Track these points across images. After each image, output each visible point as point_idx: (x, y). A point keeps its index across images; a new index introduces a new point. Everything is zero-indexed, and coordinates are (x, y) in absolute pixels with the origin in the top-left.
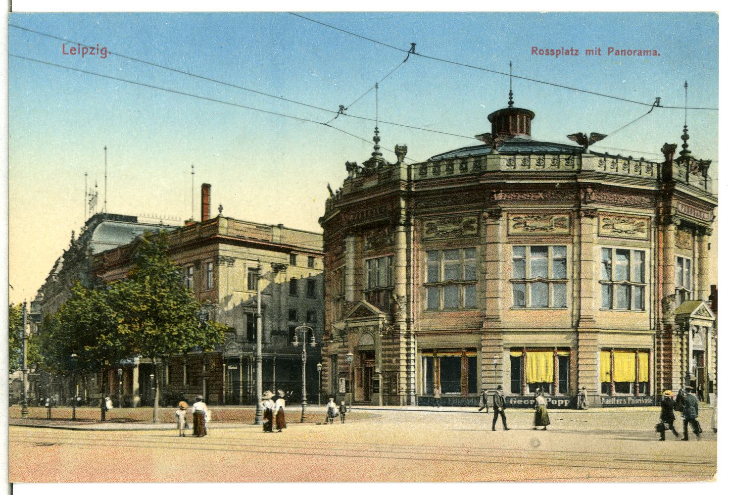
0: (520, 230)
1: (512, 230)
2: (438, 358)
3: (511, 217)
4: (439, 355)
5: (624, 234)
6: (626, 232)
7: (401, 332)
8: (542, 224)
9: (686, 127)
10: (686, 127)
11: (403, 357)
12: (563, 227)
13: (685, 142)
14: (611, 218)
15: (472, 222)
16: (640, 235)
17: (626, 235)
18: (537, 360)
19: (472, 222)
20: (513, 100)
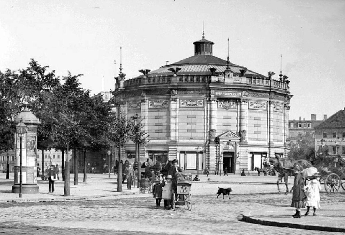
0: (184, 106)
1: (181, 106)
2: (154, 156)
3: (181, 100)
4: (155, 154)
5: (257, 108)
6: (193, 105)
7: (314, 131)
8: (195, 103)
9: (228, 57)
10: (228, 57)
11: (76, 165)
12: (201, 104)
13: (281, 77)
14: (186, 100)
15: (201, 101)
16: (263, 108)
17: (193, 106)
18: (171, 153)
19: (201, 101)
20: (205, 36)
